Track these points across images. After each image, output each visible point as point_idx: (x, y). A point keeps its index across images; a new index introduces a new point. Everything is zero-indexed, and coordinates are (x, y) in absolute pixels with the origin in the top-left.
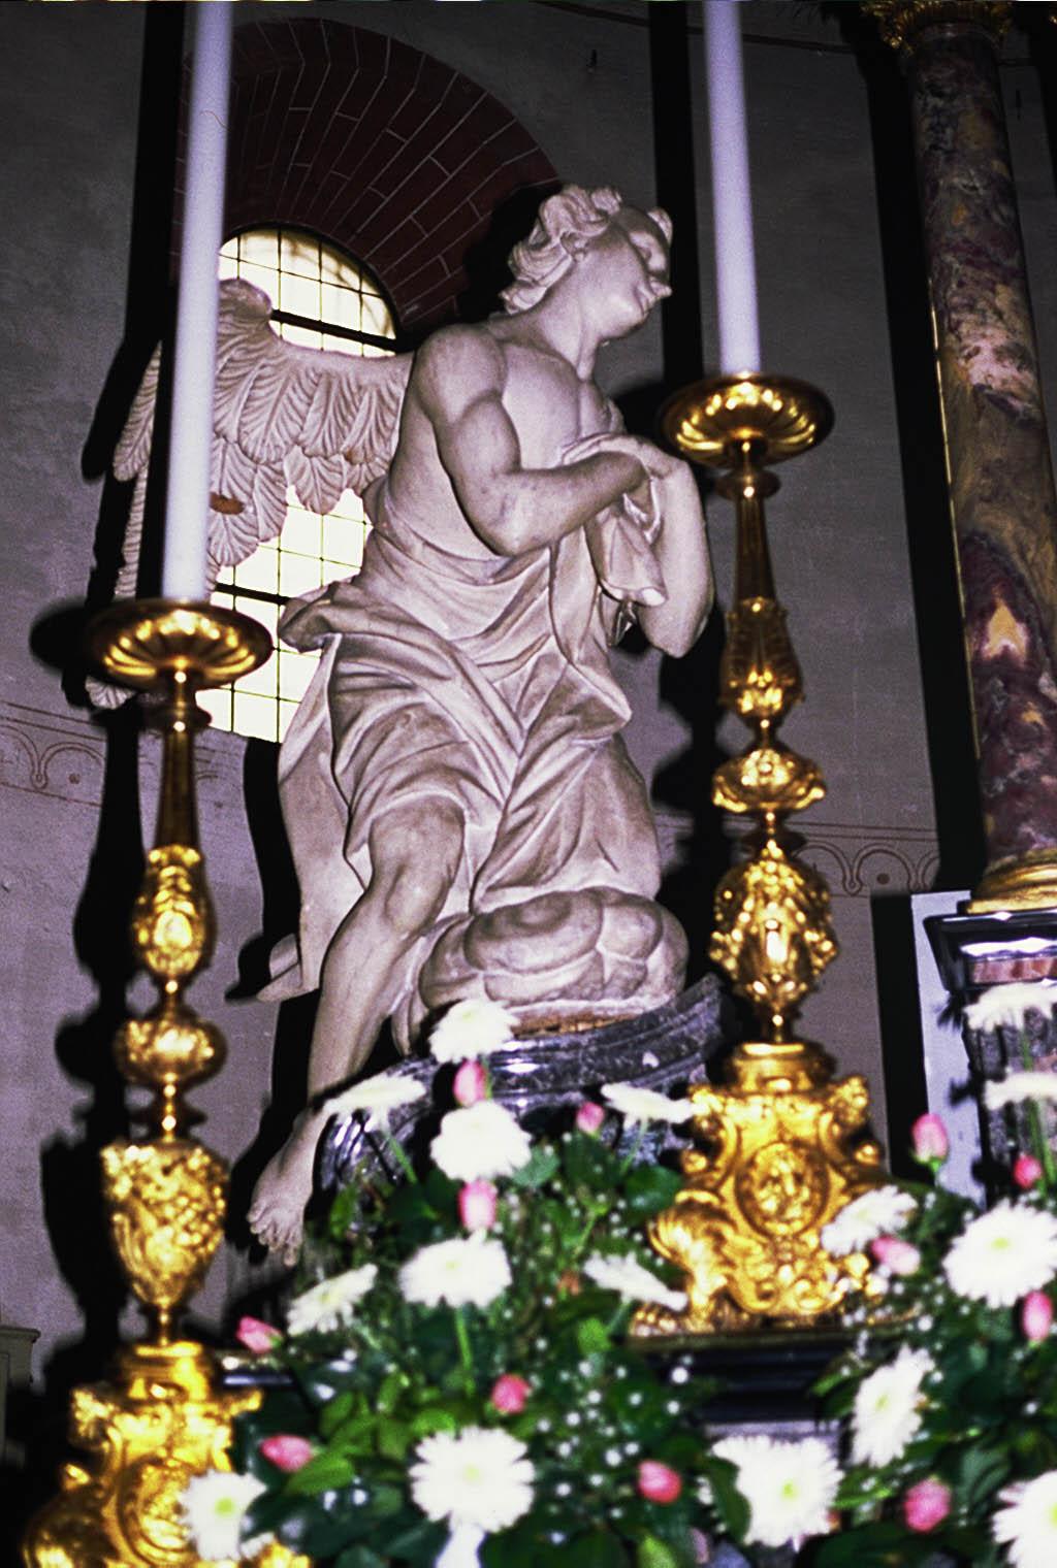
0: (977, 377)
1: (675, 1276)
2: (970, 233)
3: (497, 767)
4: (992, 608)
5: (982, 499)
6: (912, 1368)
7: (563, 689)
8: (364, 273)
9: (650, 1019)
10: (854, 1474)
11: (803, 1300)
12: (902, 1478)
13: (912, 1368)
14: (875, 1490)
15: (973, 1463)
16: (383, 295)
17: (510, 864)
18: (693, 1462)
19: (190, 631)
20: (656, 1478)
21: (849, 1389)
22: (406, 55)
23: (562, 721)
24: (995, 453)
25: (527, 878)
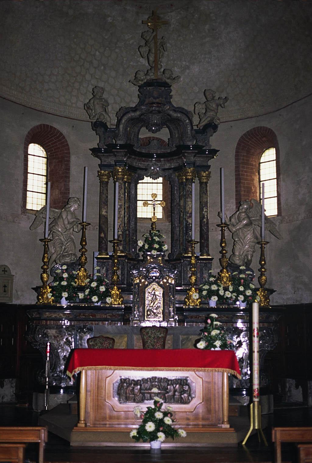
0: (103, 214)
1: (76, 283)
2: (104, 201)
3: (65, 243)
4: (101, 233)
5: (142, 46)
6: (88, 290)
7: (70, 236)
8: (43, 148)
9: (75, 262)
10: (85, 295)
11: (83, 284)
12: (87, 295)
13: (88, 290)
14: (152, 75)
15: (91, 295)
16: (46, 151)
17: (119, 426)
18: (76, 294)
19: (152, 442)
20: (74, 295)
21: (85, 291)
22: (51, 127)
23: (70, 240)
24: (103, 220)
25: (66, 252)
